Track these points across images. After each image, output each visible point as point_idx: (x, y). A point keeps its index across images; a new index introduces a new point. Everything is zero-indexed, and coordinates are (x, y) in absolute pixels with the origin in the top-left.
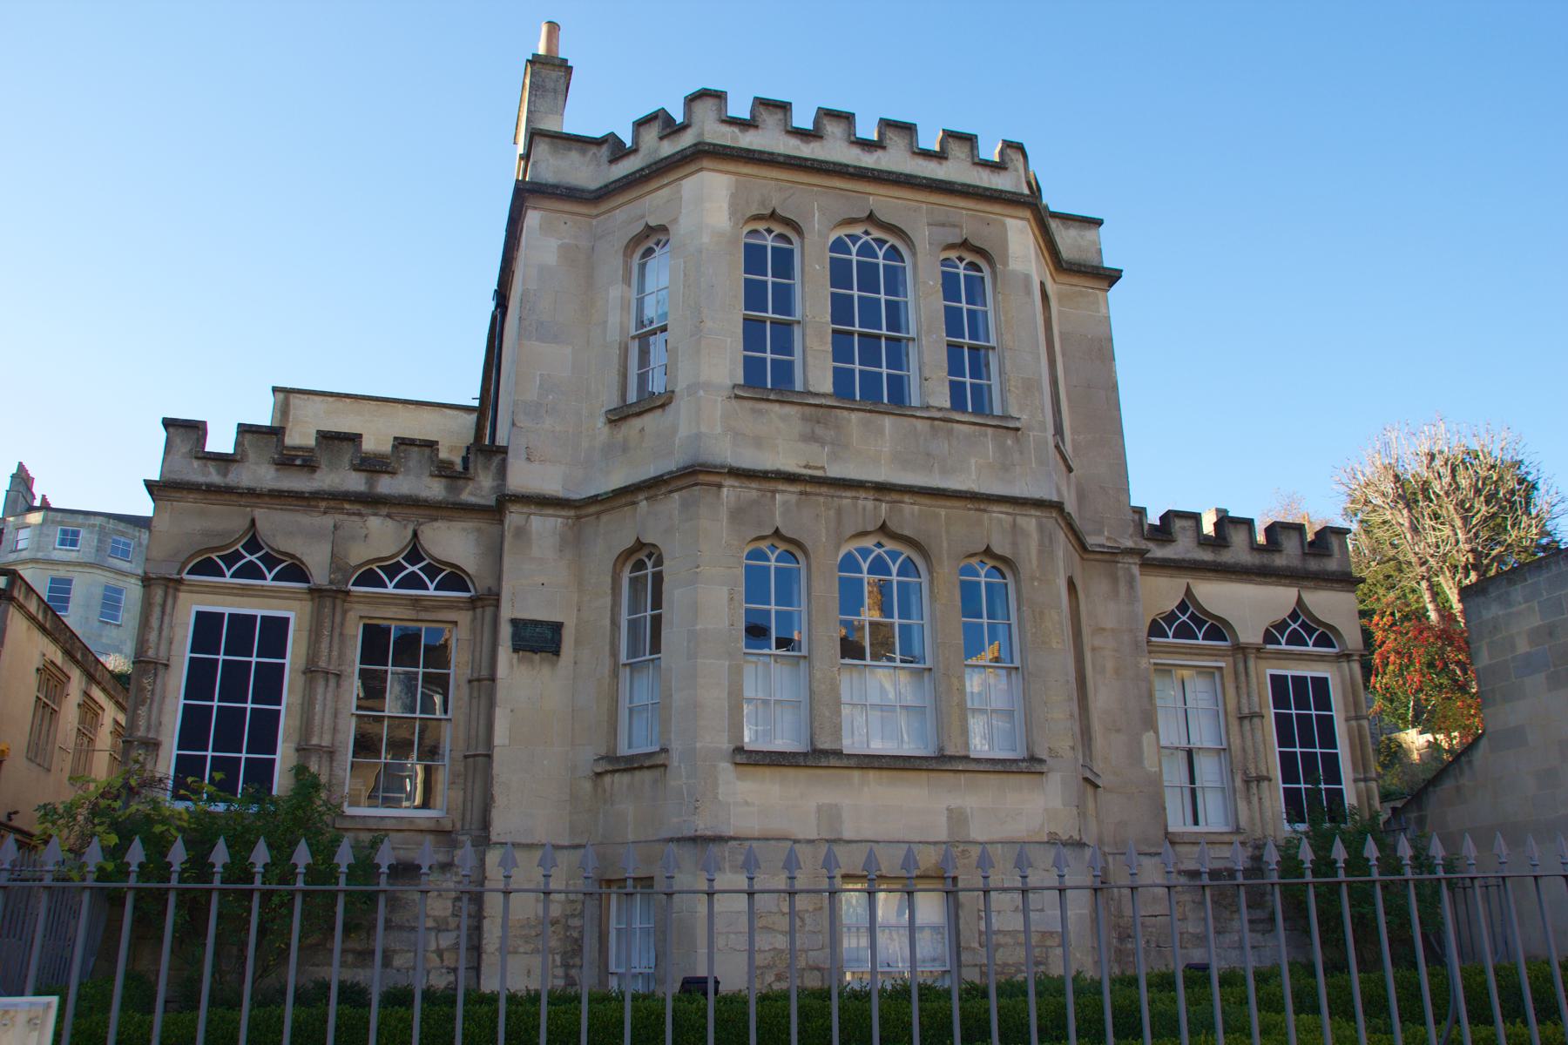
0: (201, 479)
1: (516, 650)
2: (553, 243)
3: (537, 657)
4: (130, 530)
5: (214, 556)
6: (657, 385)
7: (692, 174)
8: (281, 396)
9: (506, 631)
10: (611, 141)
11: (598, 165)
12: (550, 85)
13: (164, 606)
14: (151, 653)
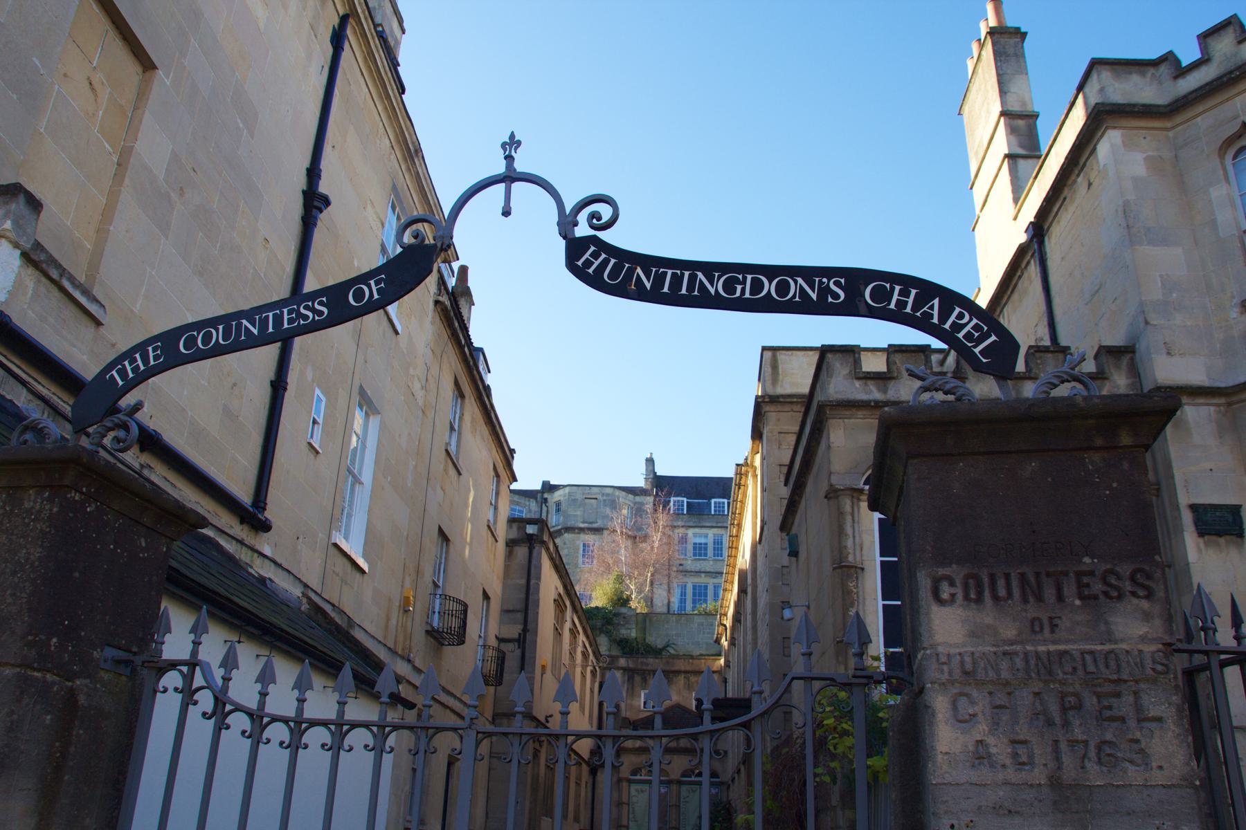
0: (865, 397)
1: (1201, 534)
2: (1139, 157)
3: (1222, 540)
4: (523, 500)
8: (768, 354)
9: (1187, 517)
10: (1169, 58)
11: (1160, 83)
12: (1011, 51)
13: (853, 514)
14: (851, 558)
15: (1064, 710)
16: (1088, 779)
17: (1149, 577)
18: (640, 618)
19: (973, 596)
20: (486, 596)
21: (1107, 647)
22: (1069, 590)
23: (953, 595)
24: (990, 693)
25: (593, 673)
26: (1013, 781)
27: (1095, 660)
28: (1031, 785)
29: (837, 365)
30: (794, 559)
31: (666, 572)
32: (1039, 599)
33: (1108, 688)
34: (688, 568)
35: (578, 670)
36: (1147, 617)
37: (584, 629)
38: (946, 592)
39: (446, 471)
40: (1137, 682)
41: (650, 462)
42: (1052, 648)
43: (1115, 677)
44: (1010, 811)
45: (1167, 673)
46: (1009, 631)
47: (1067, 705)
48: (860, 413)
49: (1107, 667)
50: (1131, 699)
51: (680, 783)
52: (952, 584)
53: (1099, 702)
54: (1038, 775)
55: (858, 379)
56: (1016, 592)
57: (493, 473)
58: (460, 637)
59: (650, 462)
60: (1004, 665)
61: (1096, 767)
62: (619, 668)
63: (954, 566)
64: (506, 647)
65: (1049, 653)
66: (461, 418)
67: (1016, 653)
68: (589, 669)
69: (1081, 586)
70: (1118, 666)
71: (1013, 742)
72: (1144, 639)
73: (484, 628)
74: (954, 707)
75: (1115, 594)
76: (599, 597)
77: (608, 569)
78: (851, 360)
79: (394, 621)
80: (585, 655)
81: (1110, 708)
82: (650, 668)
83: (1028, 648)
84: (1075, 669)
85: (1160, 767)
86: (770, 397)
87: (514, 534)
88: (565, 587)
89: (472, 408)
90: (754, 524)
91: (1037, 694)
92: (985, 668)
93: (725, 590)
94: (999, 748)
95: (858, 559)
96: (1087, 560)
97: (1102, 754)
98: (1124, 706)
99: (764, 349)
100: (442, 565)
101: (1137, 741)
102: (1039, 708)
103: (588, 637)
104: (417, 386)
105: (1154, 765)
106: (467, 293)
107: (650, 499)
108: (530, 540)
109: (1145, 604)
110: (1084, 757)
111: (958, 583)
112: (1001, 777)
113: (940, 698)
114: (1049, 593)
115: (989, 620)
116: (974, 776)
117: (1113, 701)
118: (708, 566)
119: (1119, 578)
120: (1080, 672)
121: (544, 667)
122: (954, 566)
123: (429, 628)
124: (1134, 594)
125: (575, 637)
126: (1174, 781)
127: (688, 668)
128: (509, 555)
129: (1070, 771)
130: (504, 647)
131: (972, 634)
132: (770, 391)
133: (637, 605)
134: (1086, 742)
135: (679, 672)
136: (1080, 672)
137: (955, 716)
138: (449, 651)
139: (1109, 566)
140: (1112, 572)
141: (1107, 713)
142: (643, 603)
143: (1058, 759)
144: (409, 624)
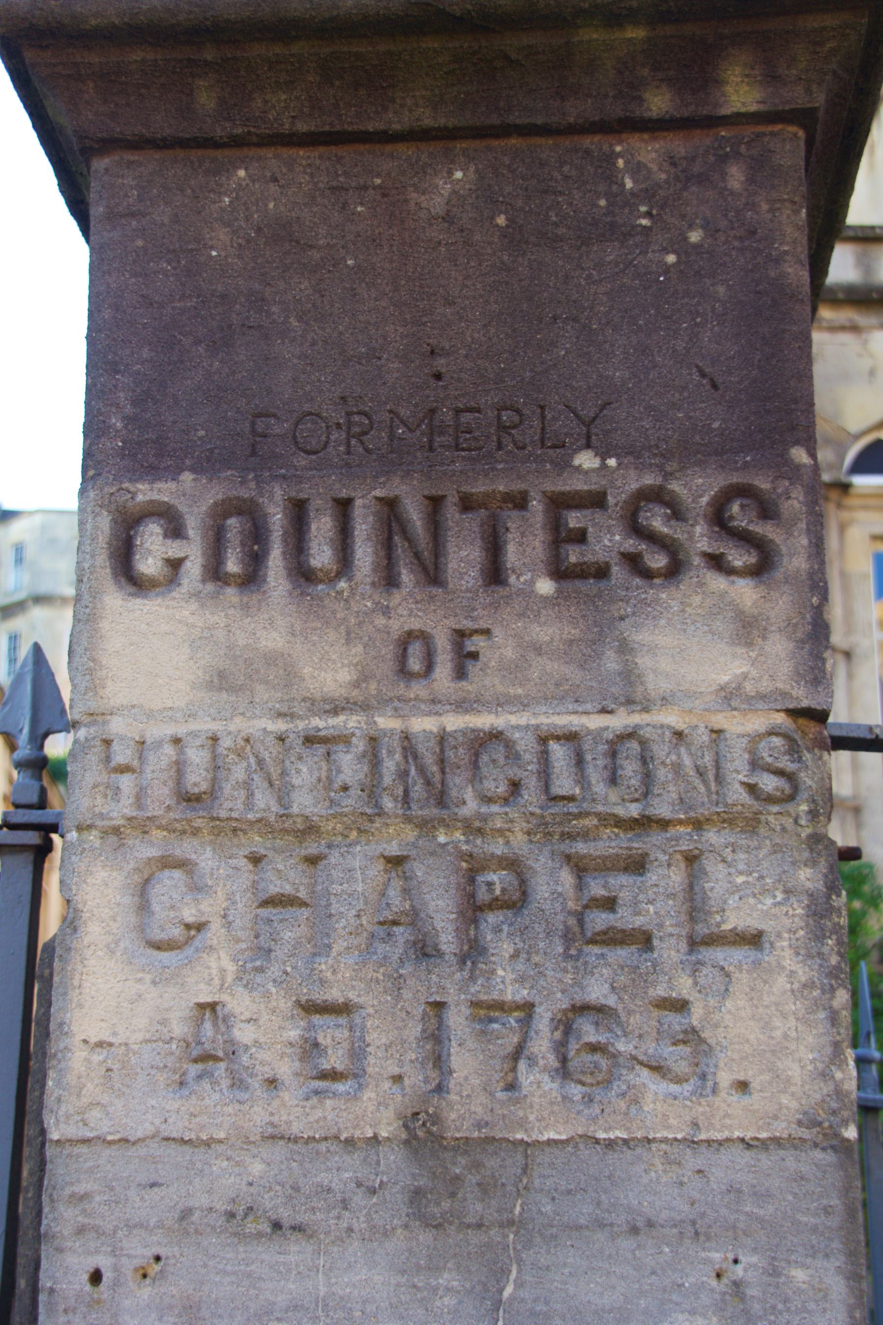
15: (472, 910)
16: (522, 1124)
17: (767, 511)
19: (232, 566)
21: (619, 721)
22: (525, 545)
23: (175, 564)
24: (256, 860)
26: (295, 1129)
27: (580, 761)
28: (350, 1142)
32: (433, 575)
33: (610, 844)
36: (748, 629)
38: (153, 550)
40: (698, 825)
42: (454, 722)
43: (634, 810)
44: (277, 1226)
45: (791, 798)
46: (331, 669)
47: (483, 895)
49: (613, 780)
50: (677, 877)
52: (175, 530)
53: (580, 886)
54: (374, 1110)
56: (365, 555)
60: (305, 773)
61: (550, 1086)
63: (187, 477)
65: (442, 738)
67: (345, 739)
69: (561, 537)
70: (648, 778)
71: (311, 1008)
72: (730, 696)
74: (143, 892)
75: (658, 561)
81: (610, 904)
83: (386, 722)
84: (515, 786)
85: (743, 1086)
91: (396, 862)
92: (247, 785)
94: (264, 1027)
96: (586, 460)
97: (573, 1046)
98: (652, 900)
101: (681, 1006)
102: (396, 901)
105: (725, 1078)
109: (745, 592)
110: (517, 1054)
111: (193, 525)
112: (258, 1115)
113: (101, 874)
114: (464, 558)
115: (273, 639)
116: (175, 1113)
117: (621, 884)
119: (677, 514)
120: (531, 796)
122: (187, 477)
124: (716, 562)
126: (781, 1129)
129: (469, 1102)
131: (221, 681)
134: (528, 1008)
136: (531, 796)
137: (141, 929)
139: (650, 479)
140: (656, 496)
141: (599, 920)
143: (439, 1061)
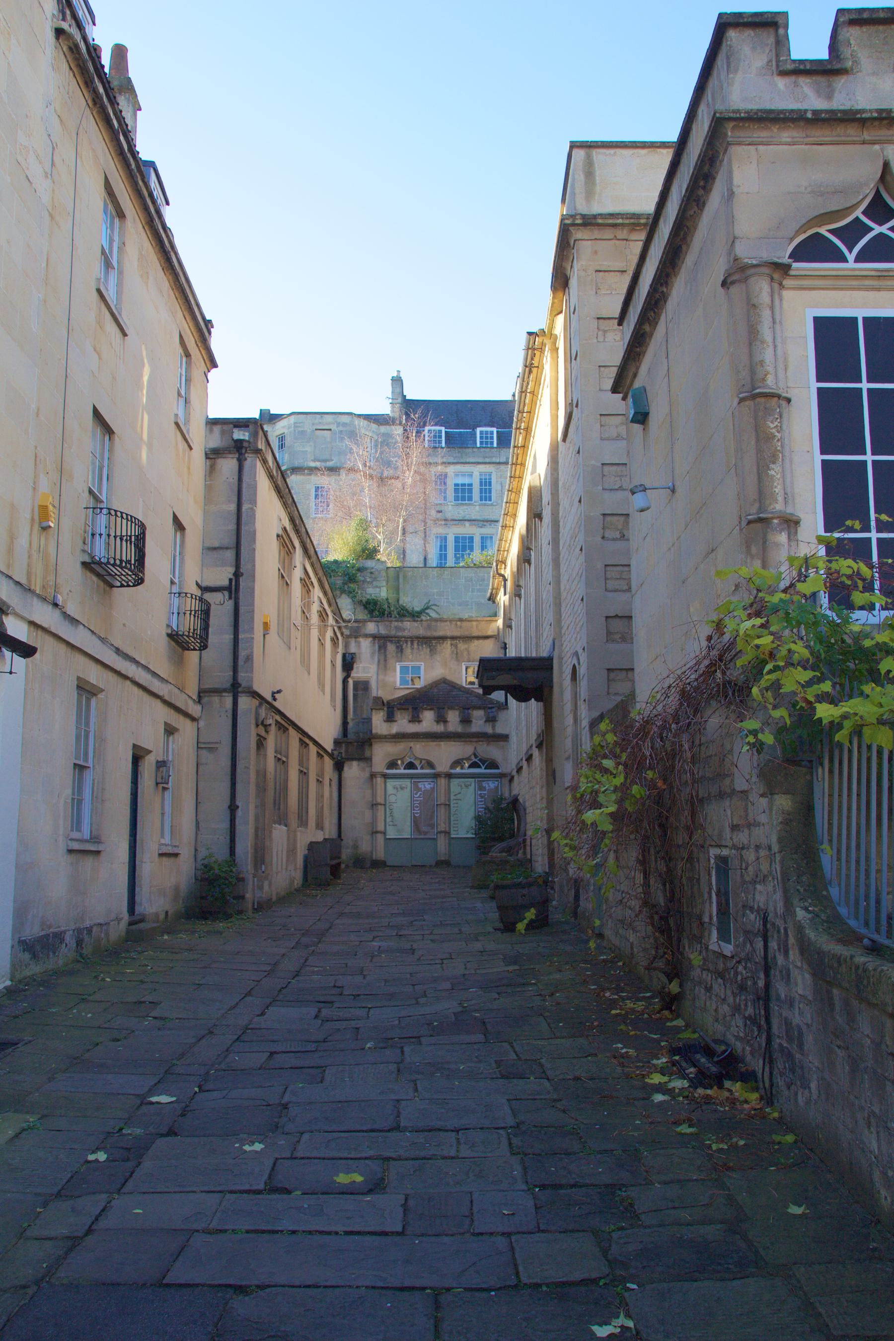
5: (823, 231)
6: (228, 465)
7: (176, 254)
8: (579, 154)
13: (772, 308)
14: (770, 381)
18: (392, 573)
20: (179, 526)
25: (335, 641)
29: (746, 50)
30: (637, 427)
31: (421, 517)
34: (449, 516)
35: (315, 633)
37: (319, 580)
39: (100, 324)
41: (397, 381)
48: (786, 135)
51: (449, 776)
55: (783, 73)
57: (180, 351)
58: (137, 570)
59: (397, 381)
62: (366, 636)
64: (214, 598)
66: (121, 249)
68: (329, 634)
73: (175, 569)
76: (337, 547)
77: (349, 514)
78: (771, 40)
79: (23, 541)
80: (323, 615)
82: (406, 634)
86: (583, 216)
87: (216, 441)
88: (292, 520)
89: (136, 239)
90: (555, 418)
93: (504, 527)
95: (781, 385)
99: (574, 145)
100: (104, 470)
103: (325, 593)
104: (36, 170)
106: (128, 87)
107: (398, 431)
108: (239, 448)
118: (474, 510)
121: (266, 625)
123: (87, 559)
125: (309, 591)
127: (456, 633)
128: (211, 470)
130: (208, 596)
132: (583, 208)
133: (387, 556)
135: (444, 638)
138: (122, 595)
142: (394, 556)
144: (52, 549)
